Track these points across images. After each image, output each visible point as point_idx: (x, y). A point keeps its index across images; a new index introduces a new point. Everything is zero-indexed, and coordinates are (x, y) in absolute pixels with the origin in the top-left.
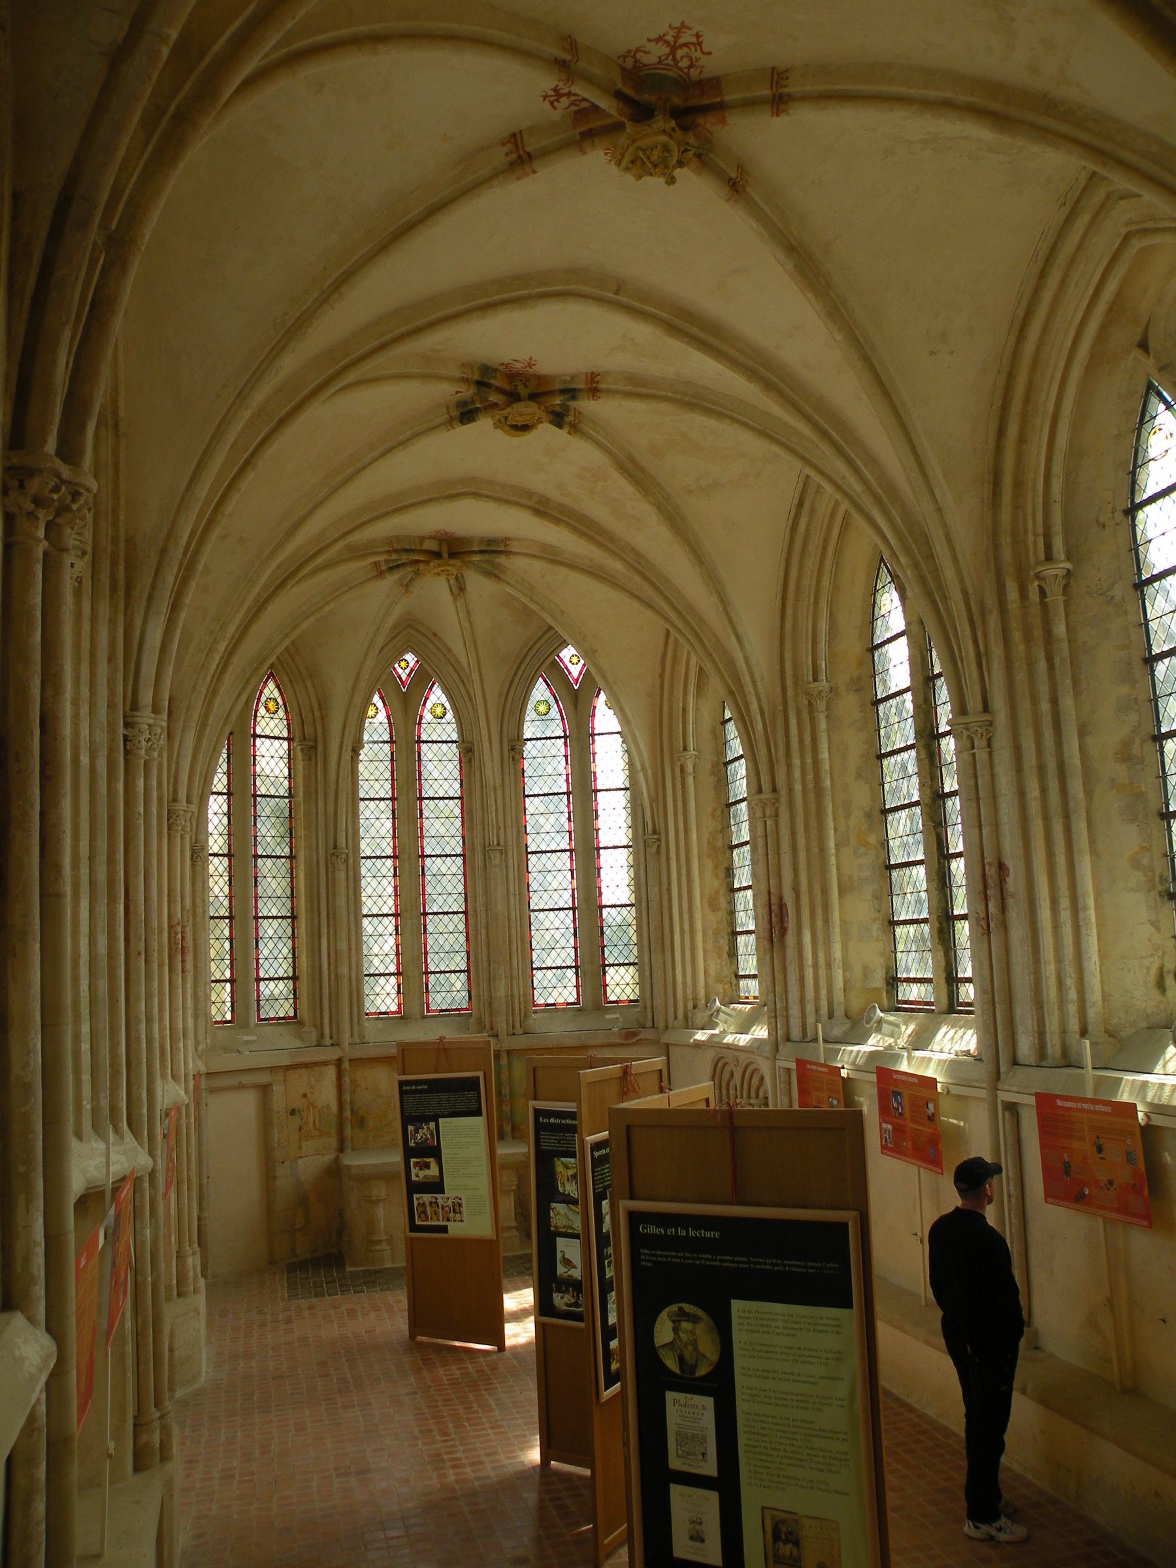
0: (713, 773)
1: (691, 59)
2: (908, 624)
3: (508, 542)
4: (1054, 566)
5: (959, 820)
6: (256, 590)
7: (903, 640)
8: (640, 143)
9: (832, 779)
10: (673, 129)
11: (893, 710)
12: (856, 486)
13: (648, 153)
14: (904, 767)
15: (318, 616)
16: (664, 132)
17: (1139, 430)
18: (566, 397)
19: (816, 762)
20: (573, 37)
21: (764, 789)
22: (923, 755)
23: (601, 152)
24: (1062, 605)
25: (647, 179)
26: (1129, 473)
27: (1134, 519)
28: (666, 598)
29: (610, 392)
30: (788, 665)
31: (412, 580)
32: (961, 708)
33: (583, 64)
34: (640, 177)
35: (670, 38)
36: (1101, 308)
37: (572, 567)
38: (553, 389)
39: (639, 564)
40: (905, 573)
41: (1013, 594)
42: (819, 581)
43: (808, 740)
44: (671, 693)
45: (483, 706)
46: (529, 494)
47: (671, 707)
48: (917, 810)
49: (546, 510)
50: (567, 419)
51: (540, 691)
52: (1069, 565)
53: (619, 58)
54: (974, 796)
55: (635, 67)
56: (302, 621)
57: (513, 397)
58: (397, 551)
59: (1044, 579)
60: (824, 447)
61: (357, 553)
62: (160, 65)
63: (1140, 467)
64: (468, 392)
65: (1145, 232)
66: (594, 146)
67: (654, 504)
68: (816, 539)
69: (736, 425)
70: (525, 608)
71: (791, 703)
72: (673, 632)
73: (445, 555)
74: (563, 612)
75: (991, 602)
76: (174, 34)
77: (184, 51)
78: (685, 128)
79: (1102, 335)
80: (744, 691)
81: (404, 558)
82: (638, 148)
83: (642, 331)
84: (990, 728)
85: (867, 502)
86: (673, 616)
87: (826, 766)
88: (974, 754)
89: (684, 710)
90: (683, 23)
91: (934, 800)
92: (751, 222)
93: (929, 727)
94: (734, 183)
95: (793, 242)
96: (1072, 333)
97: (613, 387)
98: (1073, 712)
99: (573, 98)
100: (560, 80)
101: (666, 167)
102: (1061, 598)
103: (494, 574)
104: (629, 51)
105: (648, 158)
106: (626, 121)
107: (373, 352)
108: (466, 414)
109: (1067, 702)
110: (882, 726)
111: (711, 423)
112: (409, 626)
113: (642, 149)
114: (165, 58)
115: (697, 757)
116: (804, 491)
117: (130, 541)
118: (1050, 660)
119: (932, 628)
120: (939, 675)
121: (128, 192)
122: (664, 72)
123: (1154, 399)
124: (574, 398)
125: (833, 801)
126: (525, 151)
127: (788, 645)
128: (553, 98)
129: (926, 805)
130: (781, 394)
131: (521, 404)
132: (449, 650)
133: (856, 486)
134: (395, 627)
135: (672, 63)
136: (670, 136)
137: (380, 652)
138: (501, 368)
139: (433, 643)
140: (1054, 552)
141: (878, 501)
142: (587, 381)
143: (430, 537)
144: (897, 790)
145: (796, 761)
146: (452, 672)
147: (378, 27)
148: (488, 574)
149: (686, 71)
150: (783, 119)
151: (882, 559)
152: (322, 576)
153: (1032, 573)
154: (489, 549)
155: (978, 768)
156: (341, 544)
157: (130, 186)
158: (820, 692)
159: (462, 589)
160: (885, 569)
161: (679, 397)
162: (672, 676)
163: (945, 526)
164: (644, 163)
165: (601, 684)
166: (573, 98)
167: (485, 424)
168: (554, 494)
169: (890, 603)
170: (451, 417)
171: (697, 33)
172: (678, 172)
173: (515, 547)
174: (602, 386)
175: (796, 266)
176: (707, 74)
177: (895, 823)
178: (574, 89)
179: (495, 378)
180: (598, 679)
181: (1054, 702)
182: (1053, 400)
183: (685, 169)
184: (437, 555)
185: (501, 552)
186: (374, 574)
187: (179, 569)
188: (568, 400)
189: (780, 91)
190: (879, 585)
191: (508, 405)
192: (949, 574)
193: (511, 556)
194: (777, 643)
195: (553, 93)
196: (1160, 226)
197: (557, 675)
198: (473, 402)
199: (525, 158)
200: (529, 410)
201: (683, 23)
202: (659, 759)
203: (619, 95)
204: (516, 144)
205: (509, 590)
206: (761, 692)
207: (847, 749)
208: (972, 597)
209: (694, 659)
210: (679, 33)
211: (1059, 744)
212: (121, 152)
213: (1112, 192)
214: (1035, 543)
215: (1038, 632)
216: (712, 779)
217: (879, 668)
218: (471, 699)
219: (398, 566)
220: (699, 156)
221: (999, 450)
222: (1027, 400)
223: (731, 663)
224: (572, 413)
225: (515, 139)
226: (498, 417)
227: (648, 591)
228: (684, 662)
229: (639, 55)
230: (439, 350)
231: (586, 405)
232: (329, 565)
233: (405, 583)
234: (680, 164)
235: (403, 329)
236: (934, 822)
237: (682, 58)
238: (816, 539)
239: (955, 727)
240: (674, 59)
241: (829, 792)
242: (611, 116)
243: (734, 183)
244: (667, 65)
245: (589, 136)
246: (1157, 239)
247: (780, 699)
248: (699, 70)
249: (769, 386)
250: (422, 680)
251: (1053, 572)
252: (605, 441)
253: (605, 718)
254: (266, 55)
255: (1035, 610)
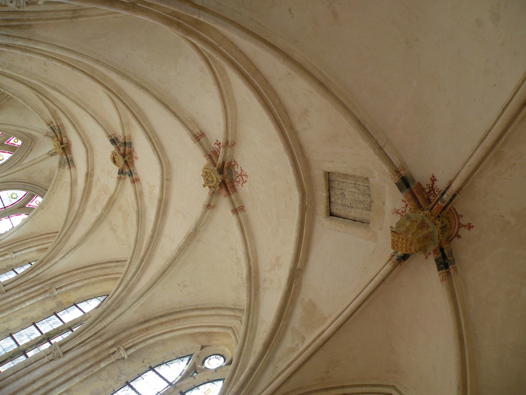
0: (7, 266)
1: (239, 182)
2: (88, 313)
3: (74, 167)
4: (124, 353)
5: (15, 364)
6: (27, 79)
7: (82, 314)
8: (212, 172)
9: (19, 310)
10: (219, 182)
11: (54, 321)
12: (128, 278)
13: (210, 176)
14: (32, 334)
15: (25, 105)
16: (217, 179)
17: (178, 358)
18: (129, 173)
19: (24, 302)
20: (236, 144)
21: (5, 287)
22: (40, 339)
23: (206, 162)
24: (112, 361)
25: (202, 178)
26: (163, 362)
27: (149, 370)
28: (70, 227)
29: (135, 187)
30: (59, 278)
31: (50, 136)
32: (61, 344)
33: (229, 149)
34: (202, 176)
35: (243, 173)
36: (209, 330)
37: (71, 191)
38: (130, 167)
39: (79, 215)
40: (105, 305)
41: (110, 343)
42: (93, 277)
43: (32, 295)
44: (36, 240)
45: (7, 174)
46: (93, 170)
47: (29, 242)
48: (16, 346)
49: (89, 177)
50: (122, 175)
51: (21, 194)
52: (126, 357)
53: (234, 160)
54: (27, 365)
55: (232, 165)
56: (22, 99)
57: (124, 156)
58: (59, 129)
59: (119, 351)
60: (138, 262)
61: (54, 114)
62: (191, 16)
63: (166, 364)
64: (121, 140)
65: (234, 332)
66: (207, 159)
67: (102, 213)
68: (107, 271)
69: (136, 231)
70: (52, 180)
71: (44, 284)
72: (57, 235)
73: (63, 146)
74: (54, 193)
75: (105, 337)
76: (201, 19)
77: (197, 23)
78: (220, 185)
79: (201, 334)
80: (44, 265)
81: (57, 132)
82: (210, 173)
83: (157, 191)
84: (57, 357)
85: (125, 283)
86: (64, 231)
87: (23, 306)
88: (45, 357)
89: (30, 247)
90: (248, 176)
91: (22, 351)
92: (200, 214)
93: (52, 336)
94: (209, 205)
95: (198, 230)
96: (199, 325)
97: (137, 188)
98: (74, 384)
99: (219, 149)
100: (223, 144)
101: (208, 183)
102: (114, 360)
103: (61, 165)
104: (236, 162)
105: (209, 177)
106: (217, 167)
107: (125, 104)
108: (114, 141)
109: (77, 380)
110: (47, 319)
111: (135, 223)
112: (32, 139)
113: (210, 174)
114: (194, 17)
115: (12, 258)
116: (122, 261)
117: (30, 26)
118: (91, 366)
119: (86, 323)
120: (72, 331)
121: (151, 8)
122: (234, 174)
123: (187, 358)
124: (129, 176)
125: (9, 314)
126: (200, 138)
127: (66, 275)
128: (217, 143)
129: (19, 349)
130: (151, 242)
131: (122, 158)
132: (27, 156)
133: (128, 278)
134: (30, 134)
135: (237, 176)
136: (217, 181)
137: (18, 131)
138: (132, 149)
139: (28, 150)
140: (129, 350)
141: (126, 286)
142: (136, 178)
143: (68, 139)
144: (22, 335)
145: (22, 294)
146: (18, 159)
147: (222, 84)
148: (60, 163)
149: (236, 181)
150: (231, 214)
151: (108, 295)
152: (41, 103)
153: (119, 346)
154: (69, 161)
155: (40, 361)
156: (55, 108)
157: (153, 9)
158: (52, 293)
159: (52, 155)
160: (105, 297)
161: (140, 210)
162: (42, 239)
163: (125, 311)
164: (207, 176)
165: (31, 214)
166: (219, 149)
167: (112, 148)
168: (95, 178)
169: (94, 303)
170: (111, 136)
171: (246, 181)
172: (207, 187)
173: (73, 170)
174: (136, 184)
175: (191, 233)
176: (237, 187)
177: (7, 341)
178: (221, 149)
179: (129, 148)
180: (32, 213)
181: (76, 375)
182: (177, 328)
183: (209, 189)
184: (62, 143)
185: (69, 165)
186: (48, 122)
187: (25, 46)
188: (128, 174)
189: (238, 210)
190: (99, 298)
191: (121, 154)
192: (109, 319)
193: (69, 169)
194: (66, 271)
195: (219, 142)
196: (236, 335)
197: (31, 197)
198: (118, 142)
199: (198, 139)
200: (121, 162)
201: (248, 176)
202: (6, 245)
203: (224, 163)
204: (201, 135)
205: (57, 172)
206: (46, 272)
207: (33, 311)
208: (104, 330)
209: (50, 244)
210: (245, 175)
211: (59, 385)
212: (163, 5)
213: (241, 317)
214: (130, 343)
215: (99, 358)
216: (5, 267)
217: (68, 309)
218: (9, 168)
219: (54, 130)
220: (214, 192)
221: (156, 318)
222: (175, 320)
223: (53, 257)
224: (124, 176)
225: (203, 134)
226: (115, 152)
227: (70, 220)
228: (49, 241)
229: (236, 165)
230: (132, 127)
231: (128, 180)
232: (47, 106)
233: (48, 134)
234: (210, 187)
235: (135, 113)
236: (12, 355)
237: (239, 178)
238: (107, 271)
239: (53, 345)
240: (238, 176)
241: (12, 311)
242: (217, 162)
243: (209, 205)
244: (236, 174)
245: (210, 157)
246: (233, 336)
247: (45, 279)
248: (237, 185)
249: (152, 237)
250: (12, 149)
251: (122, 353)
252: (118, 190)
253: (18, 220)
254: (205, 50)
255: (107, 353)
